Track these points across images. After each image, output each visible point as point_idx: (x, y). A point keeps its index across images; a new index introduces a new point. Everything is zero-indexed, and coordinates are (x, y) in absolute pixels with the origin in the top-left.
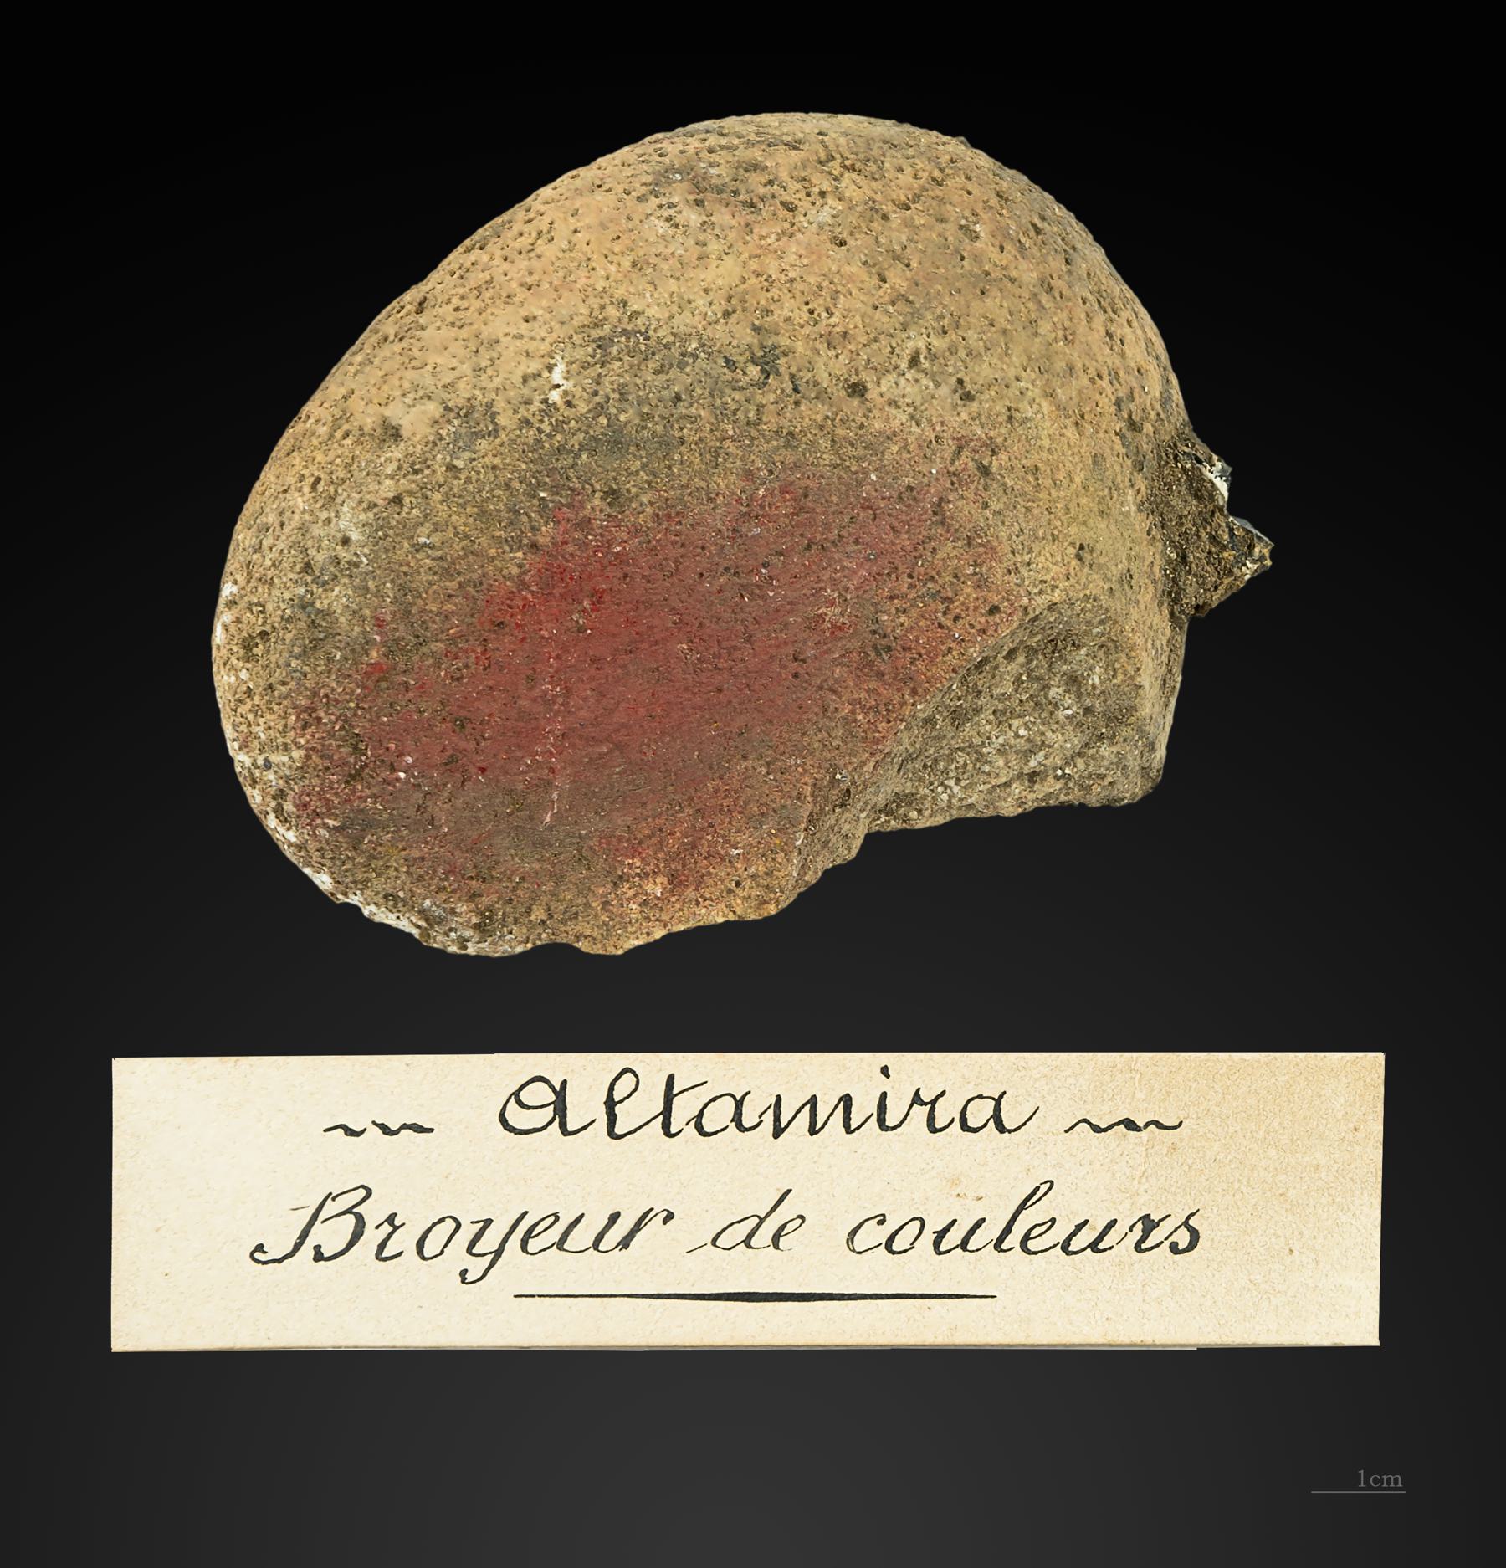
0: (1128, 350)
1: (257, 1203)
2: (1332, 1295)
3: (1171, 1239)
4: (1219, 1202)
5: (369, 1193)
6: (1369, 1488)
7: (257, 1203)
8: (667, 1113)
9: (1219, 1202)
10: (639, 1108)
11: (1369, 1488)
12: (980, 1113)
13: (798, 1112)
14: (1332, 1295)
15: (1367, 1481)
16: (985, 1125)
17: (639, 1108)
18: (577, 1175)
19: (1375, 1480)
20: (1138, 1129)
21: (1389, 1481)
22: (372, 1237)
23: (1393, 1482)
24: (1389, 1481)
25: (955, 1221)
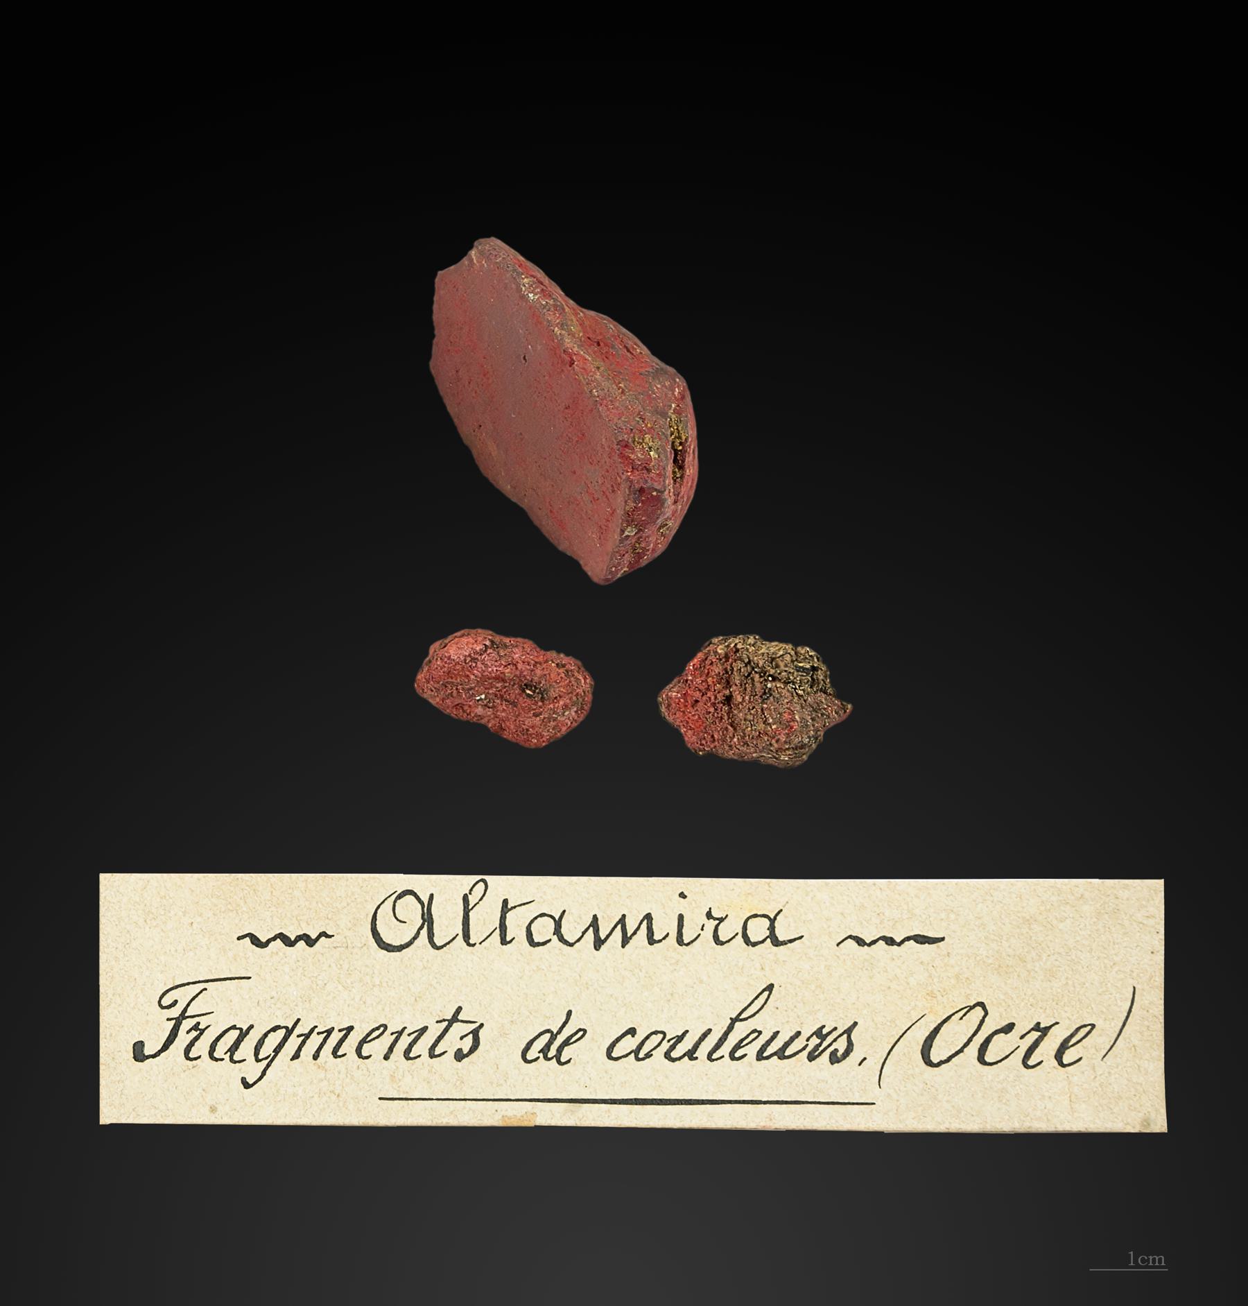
0: (679, 386)
1: (242, 996)
2: (1120, 1089)
3: (197, 1019)
4: (998, 1003)
5: (585, 1031)
6: (1137, 1266)
7: (242, 996)
8: (503, 927)
9: (998, 1003)
10: (485, 919)
11: (1137, 1266)
12: (758, 930)
13: (584, 933)
14: (1120, 1089)
15: (1136, 1261)
16: (763, 941)
17: (485, 919)
18: (415, 989)
19: (1143, 1260)
20: (884, 938)
21: (1154, 1260)
22: (183, 1039)
23: (1157, 1262)
24: (1154, 1260)
25: (299, 1020)
